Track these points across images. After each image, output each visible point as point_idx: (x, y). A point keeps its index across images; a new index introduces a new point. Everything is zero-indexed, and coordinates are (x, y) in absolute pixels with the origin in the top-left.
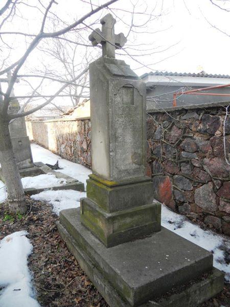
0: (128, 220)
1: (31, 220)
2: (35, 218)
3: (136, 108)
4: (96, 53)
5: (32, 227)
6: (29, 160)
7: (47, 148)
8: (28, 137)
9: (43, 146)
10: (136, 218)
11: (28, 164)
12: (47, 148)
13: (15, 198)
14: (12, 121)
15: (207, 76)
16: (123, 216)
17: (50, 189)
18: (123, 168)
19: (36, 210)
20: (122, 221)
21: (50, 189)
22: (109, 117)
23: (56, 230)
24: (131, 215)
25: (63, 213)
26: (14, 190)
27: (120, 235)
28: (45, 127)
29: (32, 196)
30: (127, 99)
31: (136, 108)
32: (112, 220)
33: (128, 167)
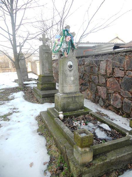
0: (46, 85)
1: (25, 90)
2: (26, 89)
3: (49, 58)
4: (41, 43)
5: (25, 91)
6: (27, 76)
7: (37, 75)
8: (26, 68)
9: (35, 74)
10: (48, 85)
11: (27, 78)
12: (37, 75)
13: (21, 49)
14: (20, 61)
15: (90, 43)
16: (45, 84)
17: (32, 84)
18: (45, 72)
19: (26, 88)
20: (45, 85)
21: (32, 84)
22: (10, 58)
23: (31, 92)
24: (47, 84)
25: (34, 88)
26: (21, 82)
27: (44, 88)
28: (36, 65)
29: (26, 86)
30: (47, 55)
31: (49, 58)
32: (42, 84)
33: (47, 72)
